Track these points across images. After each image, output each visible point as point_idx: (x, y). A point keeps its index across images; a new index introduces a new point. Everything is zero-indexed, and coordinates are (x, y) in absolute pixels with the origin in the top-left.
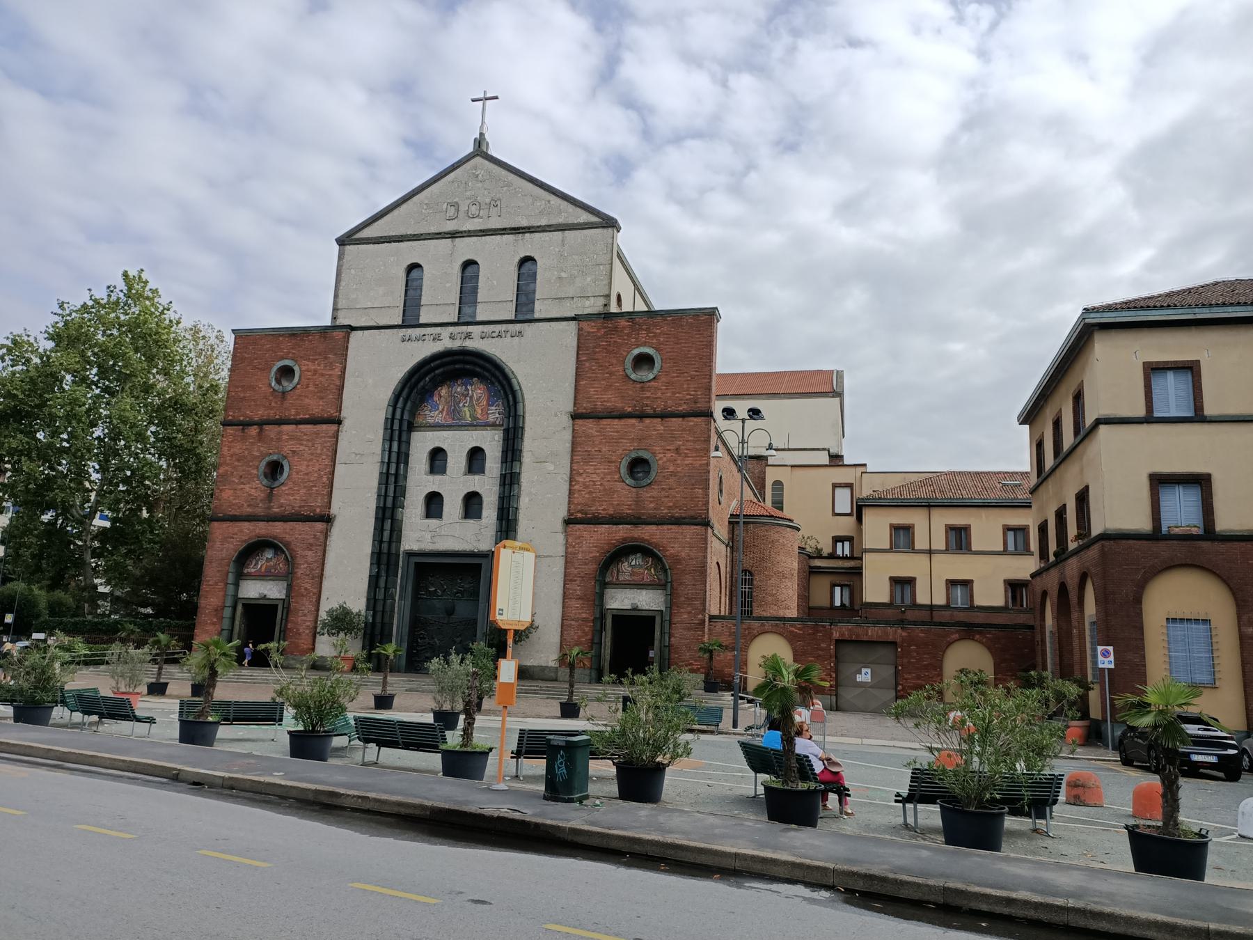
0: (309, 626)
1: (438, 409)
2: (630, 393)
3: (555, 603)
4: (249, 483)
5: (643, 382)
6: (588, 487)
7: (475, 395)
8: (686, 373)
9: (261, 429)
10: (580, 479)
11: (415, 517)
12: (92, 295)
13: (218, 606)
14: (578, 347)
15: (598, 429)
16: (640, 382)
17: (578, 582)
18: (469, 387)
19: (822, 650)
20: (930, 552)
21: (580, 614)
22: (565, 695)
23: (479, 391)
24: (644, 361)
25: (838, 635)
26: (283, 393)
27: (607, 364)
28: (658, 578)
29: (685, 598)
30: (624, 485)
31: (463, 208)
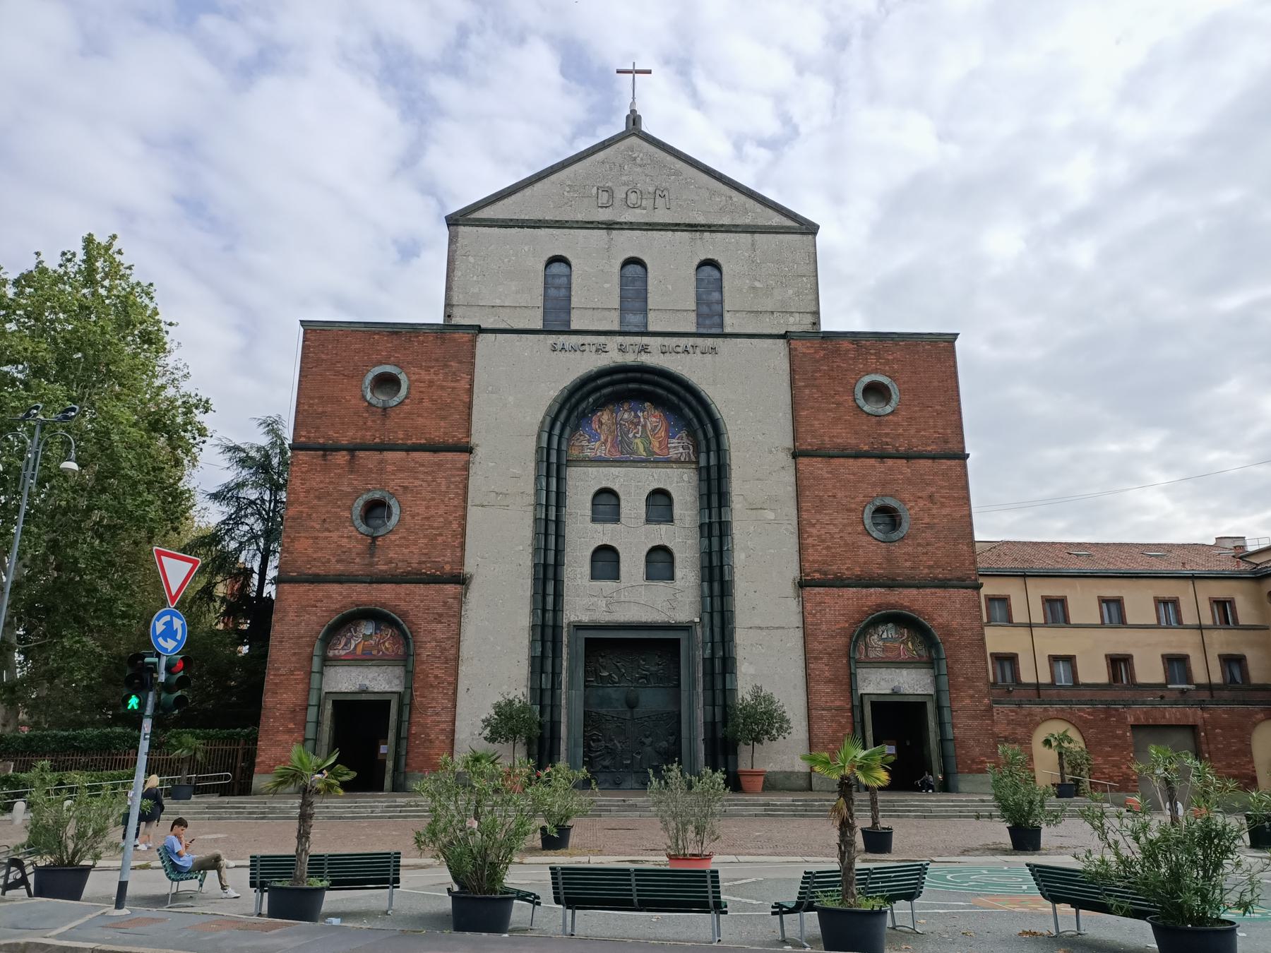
0: (445, 730)
2: (865, 428)
3: (795, 689)
4: (338, 530)
5: (879, 416)
6: (823, 541)
8: (931, 407)
9: (353, 457)
10: (814, 531)
11: (581, 578)
12: (40, 262)
13: (296, 705)
14: (792, 371)
15: (829, 469)
16: (876, 416)
17: (825, 660)
18: (640, 414)
19: (1118, 737)
20: (1030, 626)
21: (832, 702)
22: (865, 811)
24: (876, 391)
25: (1133, 719)
26: (385, 409)
27: (832, 392)
28: (918, 654)
29: (964, 678)
30: (870, 538)
31: (619, 195)
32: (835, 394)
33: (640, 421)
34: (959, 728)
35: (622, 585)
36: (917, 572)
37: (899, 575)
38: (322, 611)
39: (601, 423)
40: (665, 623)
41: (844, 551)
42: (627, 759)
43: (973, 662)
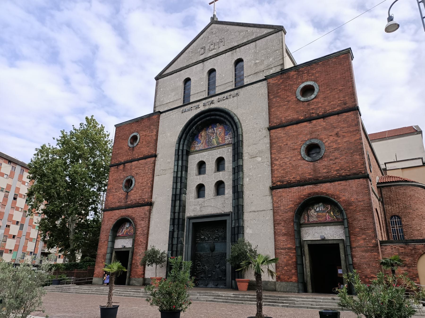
1: (201, 142)
2: (302, 109)
5: (309, 101)
7: (218, 132)
8: (336, 89)
9: (124, 166)
10: (277, 163)
14: (268, 92)
15: (284, 132)
16: (307, 101)
17: (282, 224)
21: (286, 245)
22: (253, 301)
23: (220, 129)
28: (336, 218)
32: (287, 97)
33: (215, 132)
34: (357, 257)
35: (206, 199)
36: (330, 174)
37: (320, 177)
39: (202, 136)
40: (221, 213)
41: (292, 170)
42: (210, 274)
43: (364, 220)
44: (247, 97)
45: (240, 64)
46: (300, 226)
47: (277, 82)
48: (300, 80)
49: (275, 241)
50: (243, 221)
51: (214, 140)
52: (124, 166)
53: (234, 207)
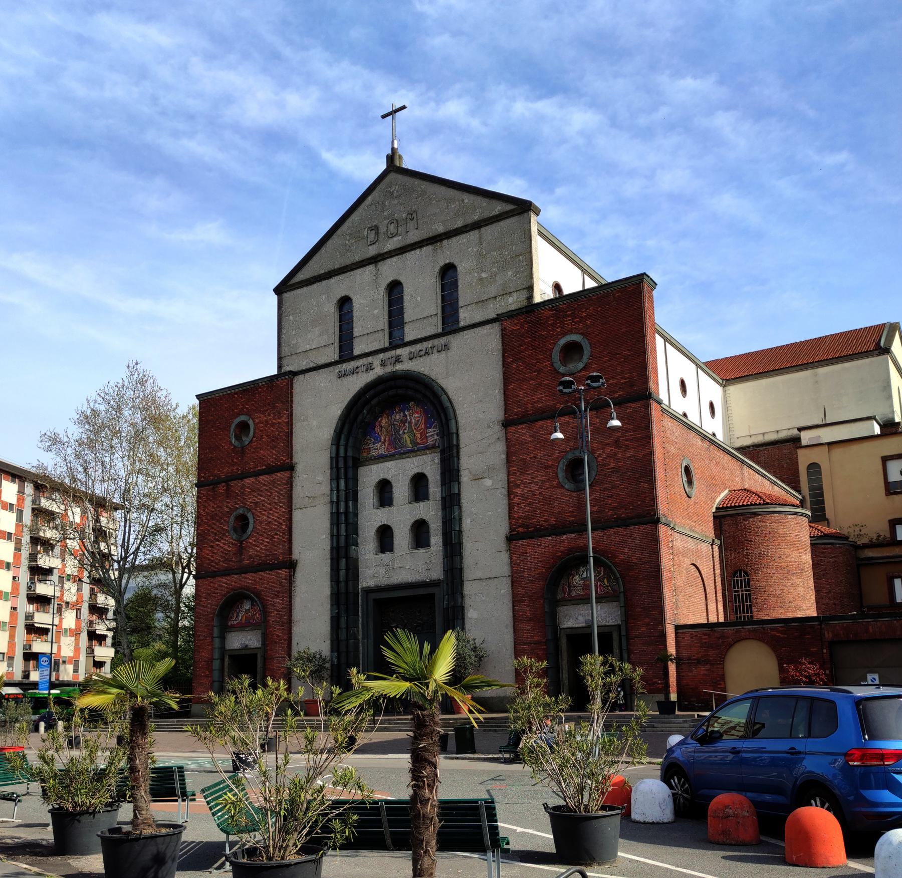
10: (519, 491)
17: (526, 603)
18: (407, 413)
21: (532, 637)
23: (416, 415)
24: (573, 350)
25: (831, 635)
29: (642, 608)
33: (407, 419)
35: (395, 555)
38: (218, 596)
39: (381, 427)
44: (465, 355)
45: (450, 273)
46: (555, 603)
47: (519, 329)
48: (559, 330)
49: (515, 632)
50: (463, 597)
51: (406, 436)
52: (228, 486)
53: (446, 571)
